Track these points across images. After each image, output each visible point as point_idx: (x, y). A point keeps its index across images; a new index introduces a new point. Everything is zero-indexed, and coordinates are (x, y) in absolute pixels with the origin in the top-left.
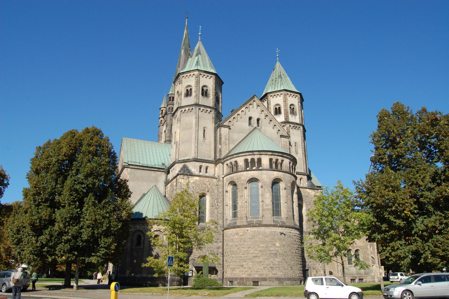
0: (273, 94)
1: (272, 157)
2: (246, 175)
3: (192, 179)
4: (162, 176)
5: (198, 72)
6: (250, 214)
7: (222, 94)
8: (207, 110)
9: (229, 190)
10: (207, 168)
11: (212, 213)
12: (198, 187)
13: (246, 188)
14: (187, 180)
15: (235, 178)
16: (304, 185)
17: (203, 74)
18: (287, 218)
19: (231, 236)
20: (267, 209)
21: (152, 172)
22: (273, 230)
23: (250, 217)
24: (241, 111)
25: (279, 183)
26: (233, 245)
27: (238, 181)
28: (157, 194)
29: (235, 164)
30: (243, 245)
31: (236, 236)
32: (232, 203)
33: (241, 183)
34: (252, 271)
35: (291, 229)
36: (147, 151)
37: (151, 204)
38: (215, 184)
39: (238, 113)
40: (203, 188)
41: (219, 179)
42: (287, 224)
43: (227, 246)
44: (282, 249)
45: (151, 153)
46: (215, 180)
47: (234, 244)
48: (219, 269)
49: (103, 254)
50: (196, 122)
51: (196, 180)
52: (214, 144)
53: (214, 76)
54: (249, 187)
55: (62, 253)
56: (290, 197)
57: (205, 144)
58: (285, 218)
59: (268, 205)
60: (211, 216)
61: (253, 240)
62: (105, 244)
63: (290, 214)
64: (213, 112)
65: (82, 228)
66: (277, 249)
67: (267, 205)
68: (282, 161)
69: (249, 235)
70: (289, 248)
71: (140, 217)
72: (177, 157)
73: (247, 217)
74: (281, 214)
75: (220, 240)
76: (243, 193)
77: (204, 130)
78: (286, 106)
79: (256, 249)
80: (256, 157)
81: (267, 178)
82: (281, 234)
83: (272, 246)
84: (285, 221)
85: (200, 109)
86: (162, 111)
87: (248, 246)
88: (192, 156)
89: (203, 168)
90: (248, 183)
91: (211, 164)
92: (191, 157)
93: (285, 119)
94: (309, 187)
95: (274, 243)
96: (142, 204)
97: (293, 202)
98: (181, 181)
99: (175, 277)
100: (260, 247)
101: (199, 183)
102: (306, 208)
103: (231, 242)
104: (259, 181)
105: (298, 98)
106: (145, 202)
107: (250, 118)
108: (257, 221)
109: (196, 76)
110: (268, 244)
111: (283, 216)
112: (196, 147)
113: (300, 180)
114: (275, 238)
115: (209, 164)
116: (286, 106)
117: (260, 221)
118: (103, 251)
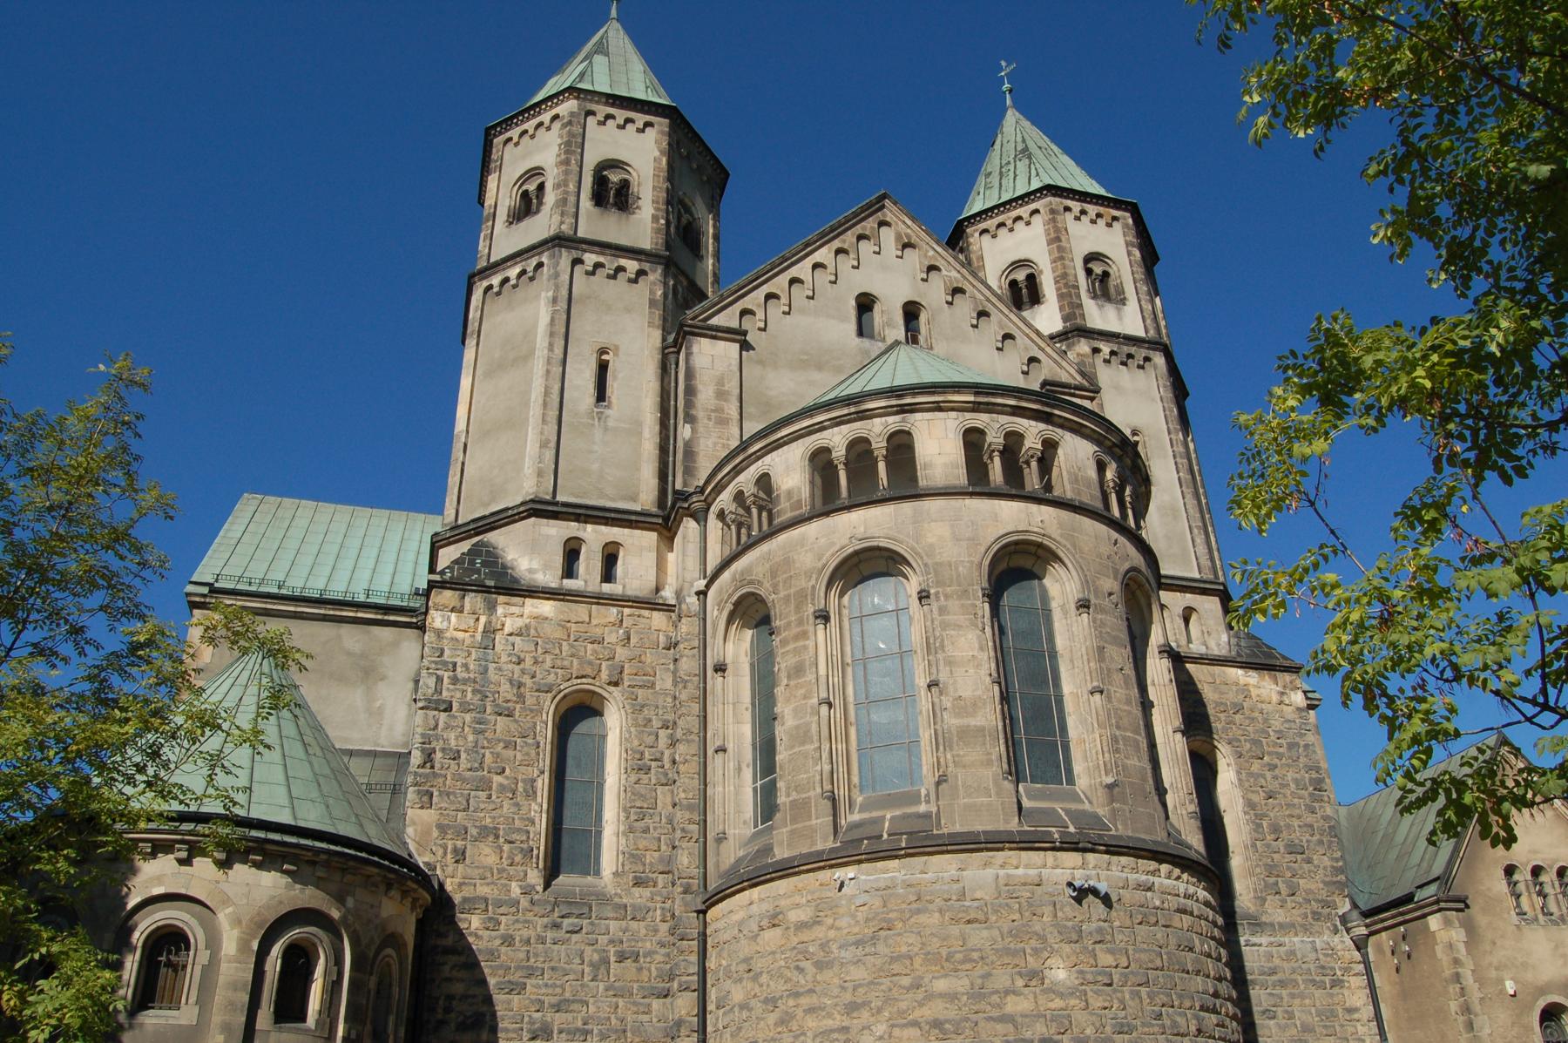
0: (990, 224)
1: (981, 420)
5: (575, 102)
6: (855, 779)
7: (717, 219)
8: (620, 269)
9: (736, 656)
10: (610, 559)
11: (638, 813)
12: (548, 658)
14: (483, 619)
15: (760, 572)
16: (1212, 644)
17: (602, 110)
18: (1110, 787)
19: (744, 942)
20: (964, 733)
21: (346, 629)
22: (1020, 871)
23: (860, 799)
24: (809, 262)
25: (1040, 579)
26: (753, 1002)
27: (775, 586)
29: (762, 494)
30: (811, 991)
31: (772, 937)
32: (754, 732)
33: (792, 591)
35: (1153, 865)
39: (794, 272)
40: (581, 664)
42: (1120, 830)
43: (721, 1012)
44: (1096, 1002)
46: (658, 619)
47: (757, 990)
50: (552, 320)
52: (657, 428)
53: (662, 123)
54: (845, 612)
56: (1120, 656)
57: (606, 429)
58: (1101, 792)
59: (975, 704)
60: (631, 830)
61: (881, 948)
63: (1133, 762)
64: (656, 275)
66: (1058, 1003)
67: (965, 707)
68: (1050, 446)
69: (853, 916)
70: (1151, 996)
73: (833, 800)
74: (1069, 771)
75: (684, 978)
76: (805, 647)
77: (603, 368)
78: (1062, 258)
79: (902, 1013)
80: (877, 430)
81: (957, 539)
82: (1078, 900)
83: (1020, 983)
84: (1102, 811)
85: (577, 261)
87: (848, 997)
91: (637, 532)
92: (512, 500)
93: (1065, 319)
94: (1239, 655)
95: (1032, 962)
97: (1146, 706)
100: (930, 997)
101: (559, 634)
102: (1238, 773)
103: (740, 980)
104: (906, 569)
105: (1126, 226)
107: (865, 304)
108: (905, 817)
110: (987, 976)
111: (1083, 781)
112: (548, 441)
113: (1187, 620)
114: (1037, 928)
115: (626, 531)
116: (1062, 258)
117: (927, 816)
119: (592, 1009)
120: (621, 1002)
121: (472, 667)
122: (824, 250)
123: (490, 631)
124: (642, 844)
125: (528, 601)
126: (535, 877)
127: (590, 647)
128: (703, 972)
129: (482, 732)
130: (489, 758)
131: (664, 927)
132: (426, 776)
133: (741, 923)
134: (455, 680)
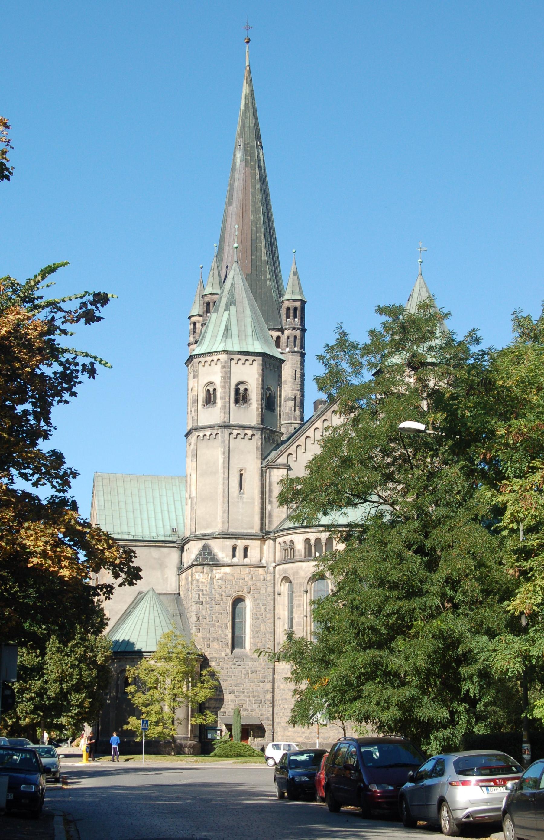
2: (307, 569)
3: (218, 571)
4: (174, 554)
8: (246, 434)
10: (246, 549)
11: (256, 632)
12: (229, 586)
13: (307, 592)
14: (210, 575)
15: (290, 572)
17: (237, 357)
28: (155, 606)
34: (311, 732)
36: (144, 501)
37: (145, 626)
38: (262, 577)
39: (307, 434)
40: (238, 587)
41: (268, 568)
45: (151, 507)
46: (261, 571)
48: (268, 727)
49: (76, 714)
51: (226, 573)
52: (260, 501)
54: (313, 588)
55: (24, 714)
60: (254, 637)
62: (77, 702)
65: (46, 682)
71: (127, 650)
72: (193, 530)
77: (241, 475)
86: (195, 324)
88: (218, 528)
89: (239, 549)
90: (310, 582)
96: (130, 624)
98: (197, 577)
99: (185, 742)
101: (232, 578)
106: (135, 621)
109: (223, 364)
112: (225, 510)
115: (251, 541)
118: (75, 711)
119: (245, 686)
120: (252, 684)
121: (208, 590)
122: (319, 422)
123: (212, 579)
124: (257, 641)
125: (222, 568)
126: (229, 651)
127: (241, 581)
128: (274, 678)
129: (212, 610)
130: (214, 618)
131: (263, 664)
132: (198, 624)
133: (283, 669)
134: (203, 595)
